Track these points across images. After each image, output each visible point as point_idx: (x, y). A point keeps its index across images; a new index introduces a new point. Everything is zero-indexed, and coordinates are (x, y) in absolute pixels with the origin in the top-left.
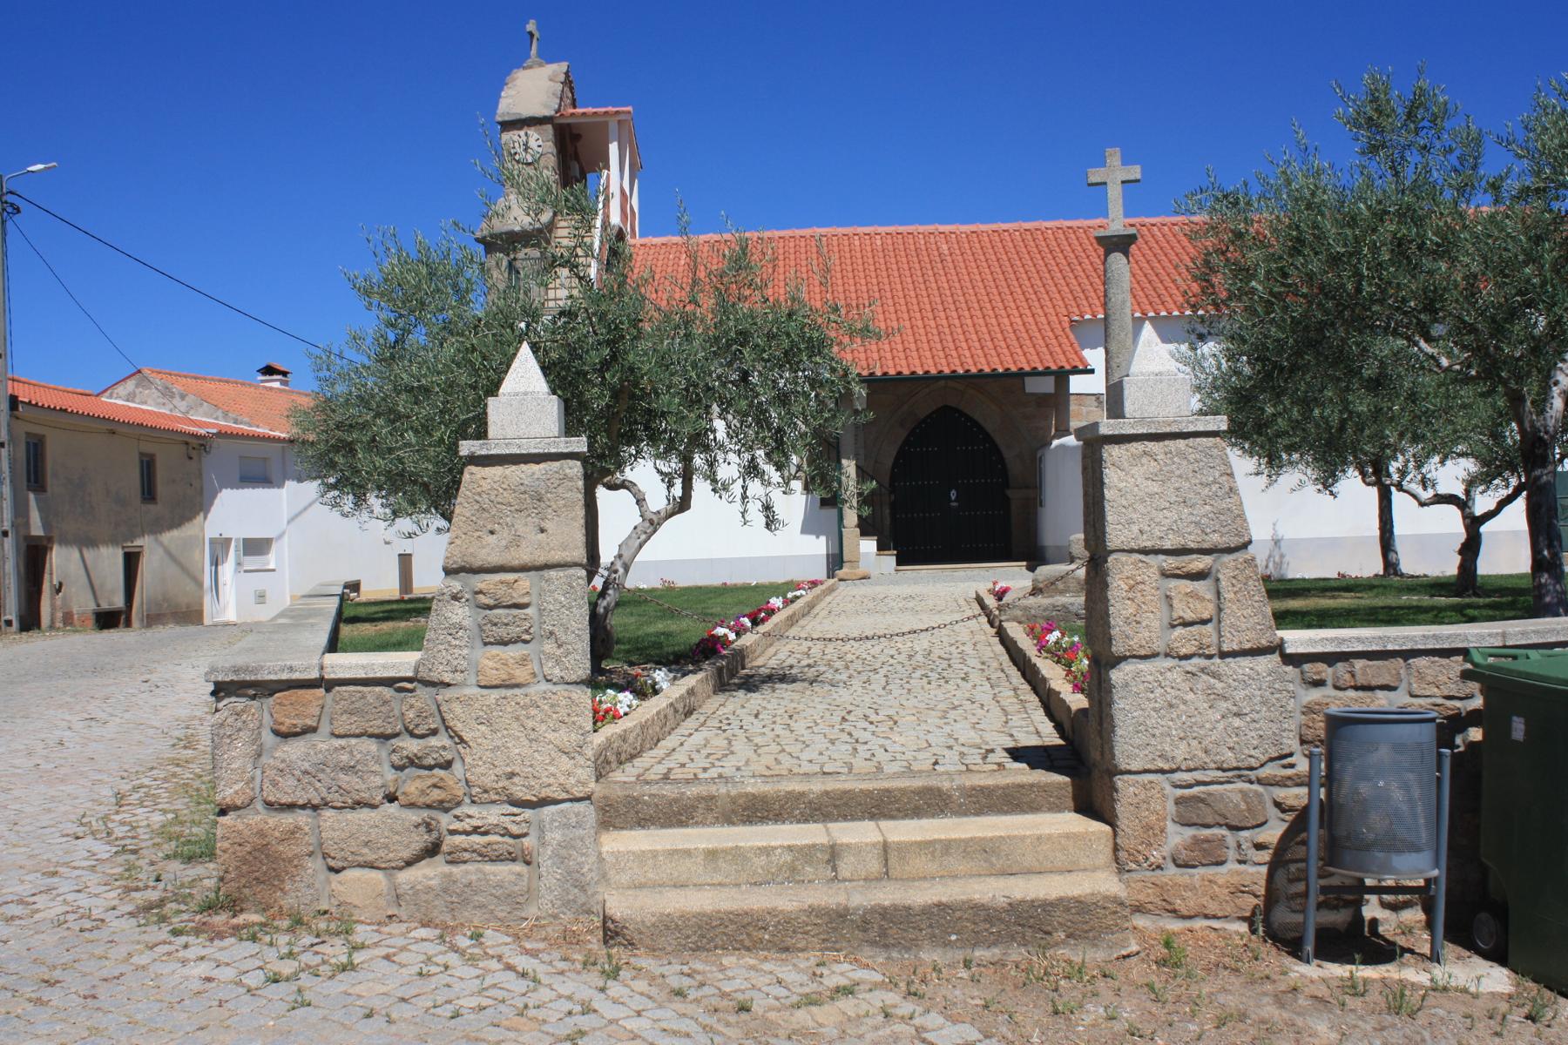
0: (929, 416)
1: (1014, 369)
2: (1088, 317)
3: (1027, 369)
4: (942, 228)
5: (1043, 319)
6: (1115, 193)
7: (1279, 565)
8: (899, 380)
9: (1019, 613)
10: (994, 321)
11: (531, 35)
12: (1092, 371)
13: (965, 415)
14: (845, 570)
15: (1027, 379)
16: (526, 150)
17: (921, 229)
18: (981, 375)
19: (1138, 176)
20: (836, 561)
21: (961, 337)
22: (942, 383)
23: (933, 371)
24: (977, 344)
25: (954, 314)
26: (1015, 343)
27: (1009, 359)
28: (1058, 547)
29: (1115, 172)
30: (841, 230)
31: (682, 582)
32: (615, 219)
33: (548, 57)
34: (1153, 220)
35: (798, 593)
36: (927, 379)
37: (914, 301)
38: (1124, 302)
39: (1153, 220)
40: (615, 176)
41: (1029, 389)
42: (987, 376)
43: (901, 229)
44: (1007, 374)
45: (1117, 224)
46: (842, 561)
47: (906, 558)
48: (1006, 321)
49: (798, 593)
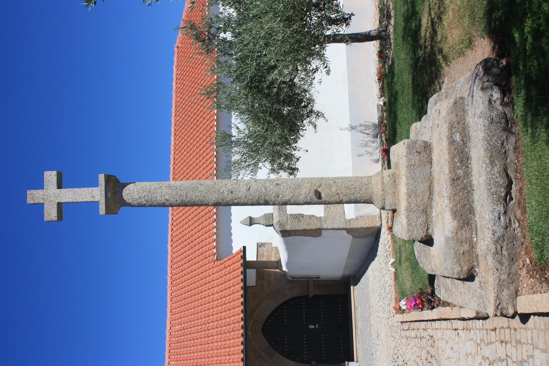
2: (215, 251)
3: (242, 284)
4: (168, 328)
5: (216, 275)
6: (69, 195)
7: (367, 127)
9: (506, 293)
10: (215, 302)
12: (244, 248)
13: (267, 319)
15: (248, 285)
17: (168, 339)
18: (245, 311)
19: (54, 173)
21: (224, 321)
22: (249, 333)
23: (242, 339)
24: (228, 312)
25: (211, 324)
26: (228, 291)
27: (236, 294)
28: (346, 267)
29: (49, 195)
34: (170, 219)
36: (246, 343)
37: (203, 346)
38: (170, 187)
39: (170, 219)
41: (254, 284)
42: (245, 307)
43: (167, 350)
44: (245, 296)
45: (96, 194)
48: (216, 296)
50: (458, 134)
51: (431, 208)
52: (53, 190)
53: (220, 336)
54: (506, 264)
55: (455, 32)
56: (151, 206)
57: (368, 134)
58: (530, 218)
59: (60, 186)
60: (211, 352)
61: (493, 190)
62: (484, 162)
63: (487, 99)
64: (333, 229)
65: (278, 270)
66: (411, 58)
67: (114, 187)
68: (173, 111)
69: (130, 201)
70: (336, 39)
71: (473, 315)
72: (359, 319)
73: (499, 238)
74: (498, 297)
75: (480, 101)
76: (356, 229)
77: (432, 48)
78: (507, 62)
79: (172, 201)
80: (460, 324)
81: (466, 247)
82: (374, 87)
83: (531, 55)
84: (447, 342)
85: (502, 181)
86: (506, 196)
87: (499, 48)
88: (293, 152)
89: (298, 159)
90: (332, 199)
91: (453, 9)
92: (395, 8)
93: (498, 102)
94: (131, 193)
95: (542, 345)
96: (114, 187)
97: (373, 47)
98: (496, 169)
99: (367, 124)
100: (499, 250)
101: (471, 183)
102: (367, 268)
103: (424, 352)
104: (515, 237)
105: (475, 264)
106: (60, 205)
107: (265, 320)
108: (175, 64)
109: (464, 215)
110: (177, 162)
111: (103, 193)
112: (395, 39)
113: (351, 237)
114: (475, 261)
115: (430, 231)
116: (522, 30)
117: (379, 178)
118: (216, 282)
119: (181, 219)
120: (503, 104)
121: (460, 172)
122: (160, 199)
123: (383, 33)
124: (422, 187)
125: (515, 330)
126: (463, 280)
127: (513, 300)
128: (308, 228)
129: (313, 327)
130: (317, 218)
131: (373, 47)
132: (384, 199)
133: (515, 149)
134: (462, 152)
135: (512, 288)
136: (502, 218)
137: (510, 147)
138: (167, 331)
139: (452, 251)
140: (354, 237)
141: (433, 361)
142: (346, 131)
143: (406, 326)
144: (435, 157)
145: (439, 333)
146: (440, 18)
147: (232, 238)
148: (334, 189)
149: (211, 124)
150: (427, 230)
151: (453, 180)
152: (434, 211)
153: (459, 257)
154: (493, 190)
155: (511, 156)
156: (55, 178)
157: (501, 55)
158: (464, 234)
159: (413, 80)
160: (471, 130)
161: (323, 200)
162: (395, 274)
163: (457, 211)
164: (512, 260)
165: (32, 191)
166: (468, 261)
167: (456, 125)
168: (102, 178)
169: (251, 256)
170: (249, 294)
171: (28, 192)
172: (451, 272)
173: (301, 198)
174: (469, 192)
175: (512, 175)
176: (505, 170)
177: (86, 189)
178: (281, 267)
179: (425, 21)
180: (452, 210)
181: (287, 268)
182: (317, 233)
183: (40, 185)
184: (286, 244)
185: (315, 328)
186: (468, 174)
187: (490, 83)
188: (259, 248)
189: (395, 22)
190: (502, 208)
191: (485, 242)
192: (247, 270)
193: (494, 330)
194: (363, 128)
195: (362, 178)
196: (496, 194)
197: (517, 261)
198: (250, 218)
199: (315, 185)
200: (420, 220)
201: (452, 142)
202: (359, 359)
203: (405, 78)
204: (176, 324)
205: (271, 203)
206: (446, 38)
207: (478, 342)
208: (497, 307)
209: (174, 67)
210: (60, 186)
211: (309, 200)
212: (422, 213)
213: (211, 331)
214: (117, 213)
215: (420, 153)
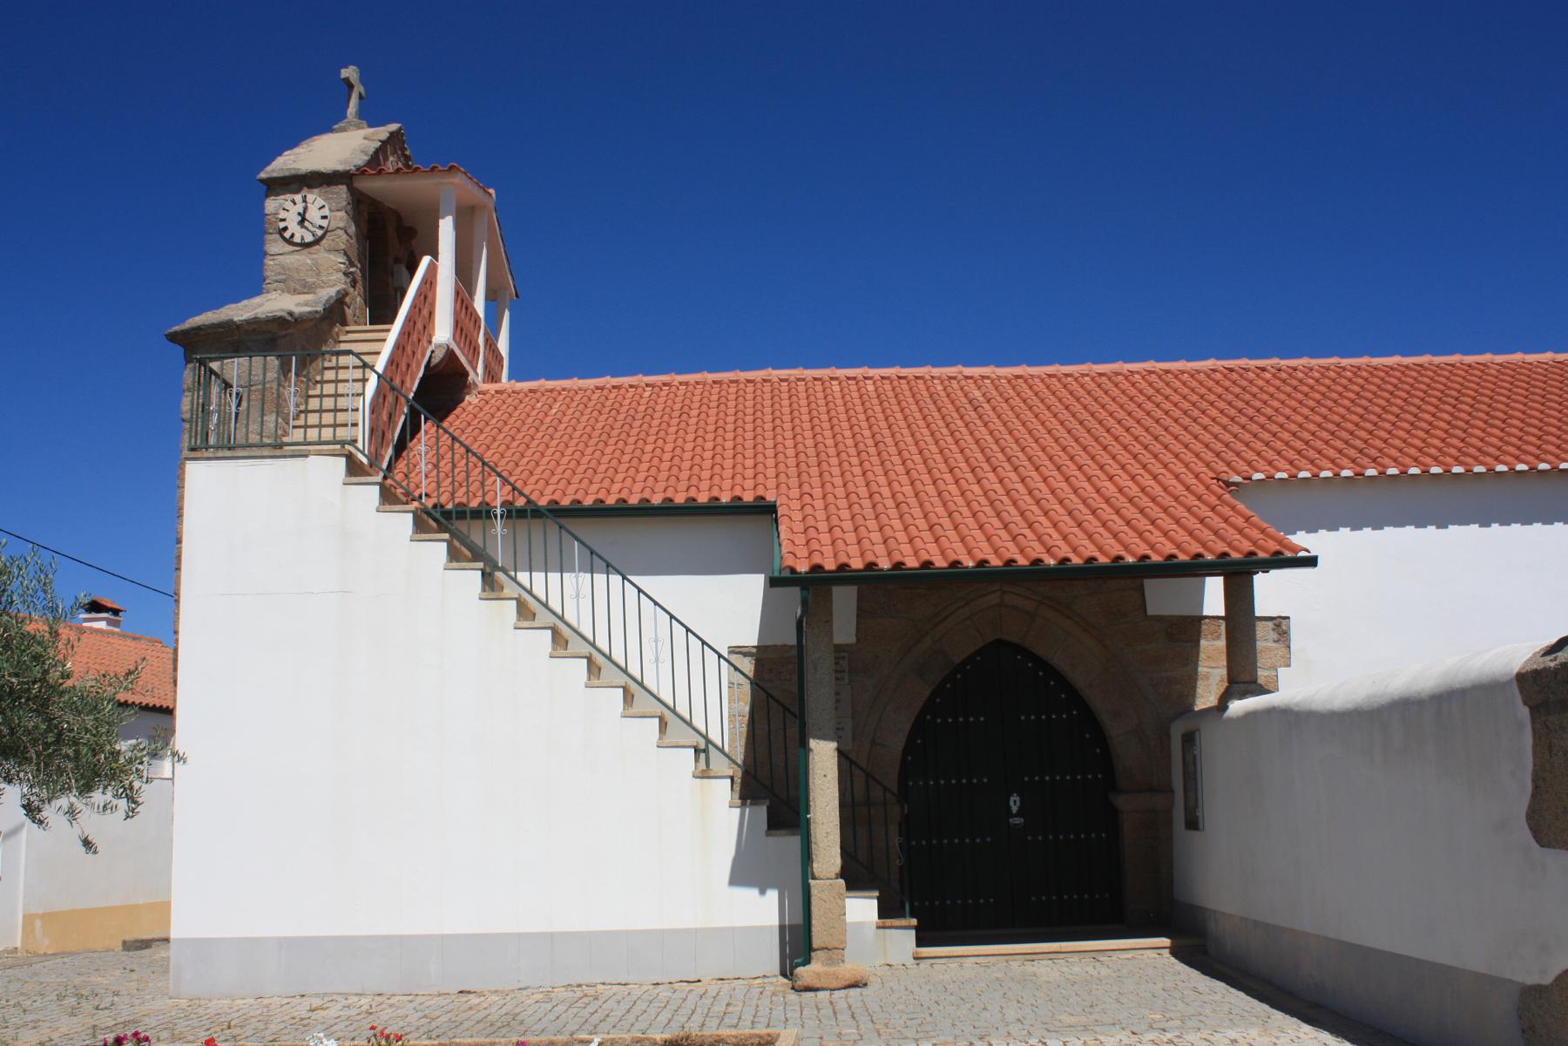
8: (927, 581)
11: (347, 82)
12: (1312, 562)
17: (936, 371)
20: (797, 944)
32: (443, 332)
33: (370, 116)
43: (904, 372)
44: (1117, 570)
46: (810, 949)
47: (936, 929)
129: (1015, 809)
138: (960, 368)
178: (1242, 696)
181: (1251, 716)
185: (1009, 813)
188: (1270, 624)
202: (924, 965)
204: (984, 389)
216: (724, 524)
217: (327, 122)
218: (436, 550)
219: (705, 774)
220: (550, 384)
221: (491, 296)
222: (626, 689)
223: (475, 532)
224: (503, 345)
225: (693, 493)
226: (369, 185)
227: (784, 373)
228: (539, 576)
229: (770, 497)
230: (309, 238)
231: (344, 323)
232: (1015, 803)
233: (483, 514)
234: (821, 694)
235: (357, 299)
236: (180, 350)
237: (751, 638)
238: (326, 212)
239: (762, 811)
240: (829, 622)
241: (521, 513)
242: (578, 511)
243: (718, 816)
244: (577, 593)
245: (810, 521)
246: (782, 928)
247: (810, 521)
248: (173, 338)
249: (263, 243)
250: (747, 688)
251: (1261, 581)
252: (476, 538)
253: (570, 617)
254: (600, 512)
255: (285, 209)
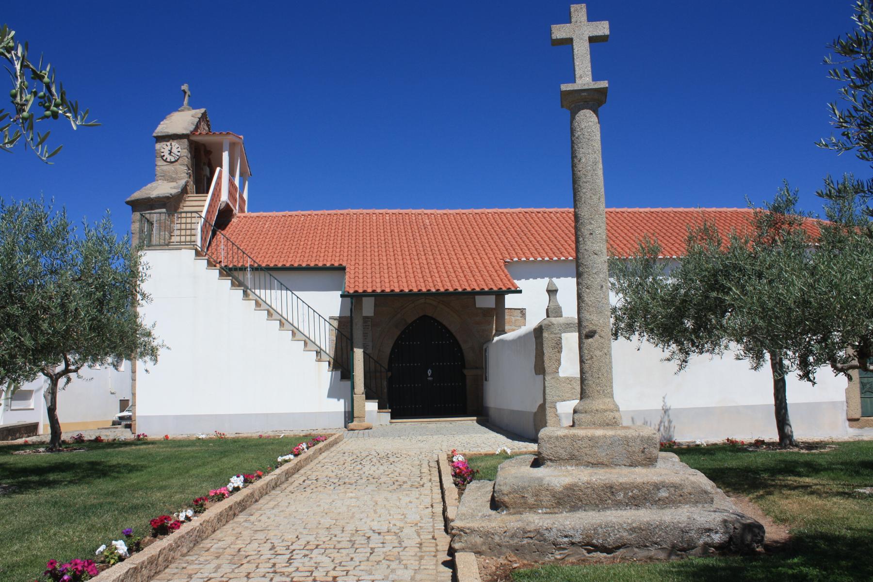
0: (415, 322)
1: (469, 289)
2: (516, 259)
3: (478, 289)
7: (668, 429)
9: (479, 540)
10: (456, 262)
12: (520, 292)
14: (354, 423)
15: (477, 298)
16: (170, 154)
17: (414, 211)
18: (447, 293)
20: (350, 416)
21: (435, 271)
24: (445, 275)
25: (431, 257)
30: (365, 211)
31: (230, 433)
32: (224, 197)
33: (193, 105)
35: (287, 457)
37: (406, 249)
40: (223, 172)
43: (401, 211)
44: (465, 293)
45: (584, 77)
46: (353, 417)
48: (464, 261)
49: (287, 457)
50: (667, 495)
51: (577, 465)
52: (586, 33)
53: (418, 267)
54: (511, 542)
55: (796, 506)
56: (572, 142)
57: (659, 430)
58: (566, 568)
59: (592, 40)
60: (400, 258)
61: (600, 530)
62: (634, 521)
63: (712, 526)
64: (544, 387)
65: (494, 332)
66: (757, 467)
67: (593, 100)
68: (681, 209)
69: (577, 118)
70: (779, 370)
71: (450, 514)
72: (438, 425)
73: (542, 535)
74: (473, 531)
75: (710, 519)
76: (545, 415)
77: (772, 486)
78: (759, 553)
79: (580, 167)
80: (439, 509)
81: (531, 500)
82: (719, 438)
83: (771, 573)
84: (417, 498)
85: (611, 541)
86: (593, 545)
87: (777, 547)
88: (636, 333)
89: (629, 338)
90: (586, 351)
91: (825, 505)
92: (822, 454)
93: (708, 540)
94: (588, 122)
95: (418, 577)
96: (593, 100)
97: (772, 435)
98: (625, 534)
99: (672, 429)
100: (529, 535)
101: (608, 508)
102: (498, 432)
103: (406, 479)
104: (543, 553)
105: (512, 511)
106: (569, 41)
107: (438, 319)
108: (739, 210)
109: (569, 499)
110: (619, 215)
111: (586, 87)
112: (781, 454)
113: (535, 410)
114: (515, 510)
115: (549, 463)
116: (802, 565)
117: (612, 407)
118: (479, 261)
119: (551, 221)
120: (707, 546)
121: (621, 496)
122: (581, 152)
123: (788, 442)
124: (602, 455)
125: (435, 556)
126: (493, 498)
127: (470, 548)
128: (546, 358)
130: (557, 369)
131: (772, 435)
132: (586, 412)
133: (651, 558)
134: (645, 499)
135: (484, 548)
136: (566, 540)
137: (652, 552)
139: (526, 484)
140: (535, 414)
141: (395, 487)
142: (662, 403)
143: (435, 464)
144: (638, 470)
145: (428, 492)
146: (812, 493)
147: (531, 280)
148: (598, 353)
149: (666, 253)
150: (551, 460)
151: (611, 487)
152: (573, 468)
153: (519, 492)
154: (600, 530)
155: (642, 553)
156: (600, 33)
157: (767, 547)
158: (546, 499)
159: (731, 469)
160: (673, 510)
161: (584, 341)
162: (493, 455)
163: (574, 490)
164: (517, 550)
165: (585, 10)
166: (515, 502)
167: (678, 492)
168: (604, 84)
169: (511, 301)
170: (464, 299)
171: (584, 5)
172: (502, 483)
173: (586, 315)
174: (597, 506)
175: (618, 553)
176: (624, 546)
177: (590, 69)
179: (807, 480)
180: (575, 485)
181: (497, 341)
182: (540, 369)
183: (592, 17)
184: (526, 336)
186: (618, 505)
187: (732, 531)
189: (803, 454)
190: (578, 540)
191: (536, 520)
192: (494, 297)
193: (434, 538)
194: (666, 424)
195: (612, 387)
196: (595, 533)
197: (516, 555)
198: (556, 291)
199: (602, 330)
200: (562, 451)
201: (657, 487)
202: (393, 425)
203: (732, 462)
205: (580, 280)
206: (787, 498)
207: (419, 524)
208: (462, 530)
209: (735, 209)
210: (592, 40)
211: (584, 324)
212: (570, 453)
213: (424, 257)
214: (562, 106)
215: (643, 452)
216: (328, 274)
217: (176, 107)
218: (227, 283)
219: (319, 360)
220: (265, 214)
221: (241, 175)
222: (293, 332)
223: (240, 275)
224: (245, 196)
225: (317, 263)
226: (194, 138)
227: (355, 211)
228: (263, 291)
229: (344, 264)
230: (173, 160)
231: (187, 193)
232: (429, 372)
233: (243, 269)
234: (358, 334)
235: (192, 187)
236: (130, 207)
237: (337, 314)
238: (179, 149)
239: (339, 373)
240: (361, 309)
241: (257, 269)
242: (276, 269)
243: (324, 375)
244: (275, 297)
245: (357, 274)
246: (345, 412)
247: (357, 274)
248: (128, 203)
249: (155, 161)
250: (334, 332)
251: (508, 297)
252: (241, 278)
253: (274, 306)
254: (284, 269)
255: (164, 148)
